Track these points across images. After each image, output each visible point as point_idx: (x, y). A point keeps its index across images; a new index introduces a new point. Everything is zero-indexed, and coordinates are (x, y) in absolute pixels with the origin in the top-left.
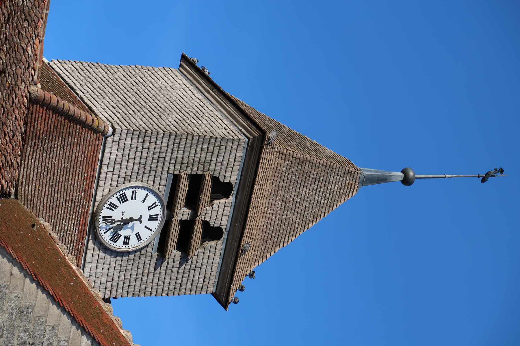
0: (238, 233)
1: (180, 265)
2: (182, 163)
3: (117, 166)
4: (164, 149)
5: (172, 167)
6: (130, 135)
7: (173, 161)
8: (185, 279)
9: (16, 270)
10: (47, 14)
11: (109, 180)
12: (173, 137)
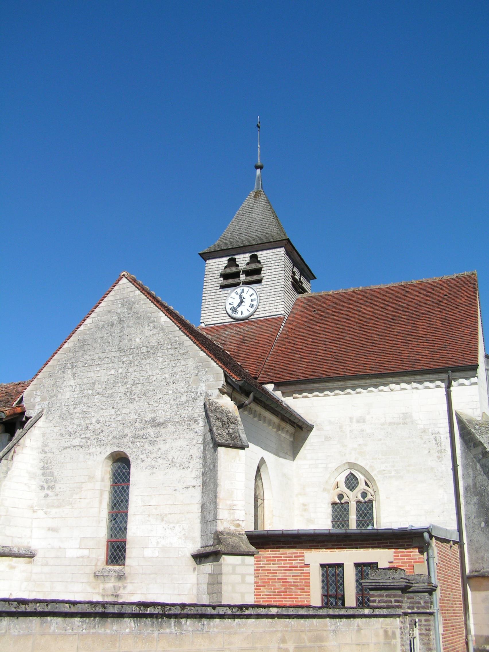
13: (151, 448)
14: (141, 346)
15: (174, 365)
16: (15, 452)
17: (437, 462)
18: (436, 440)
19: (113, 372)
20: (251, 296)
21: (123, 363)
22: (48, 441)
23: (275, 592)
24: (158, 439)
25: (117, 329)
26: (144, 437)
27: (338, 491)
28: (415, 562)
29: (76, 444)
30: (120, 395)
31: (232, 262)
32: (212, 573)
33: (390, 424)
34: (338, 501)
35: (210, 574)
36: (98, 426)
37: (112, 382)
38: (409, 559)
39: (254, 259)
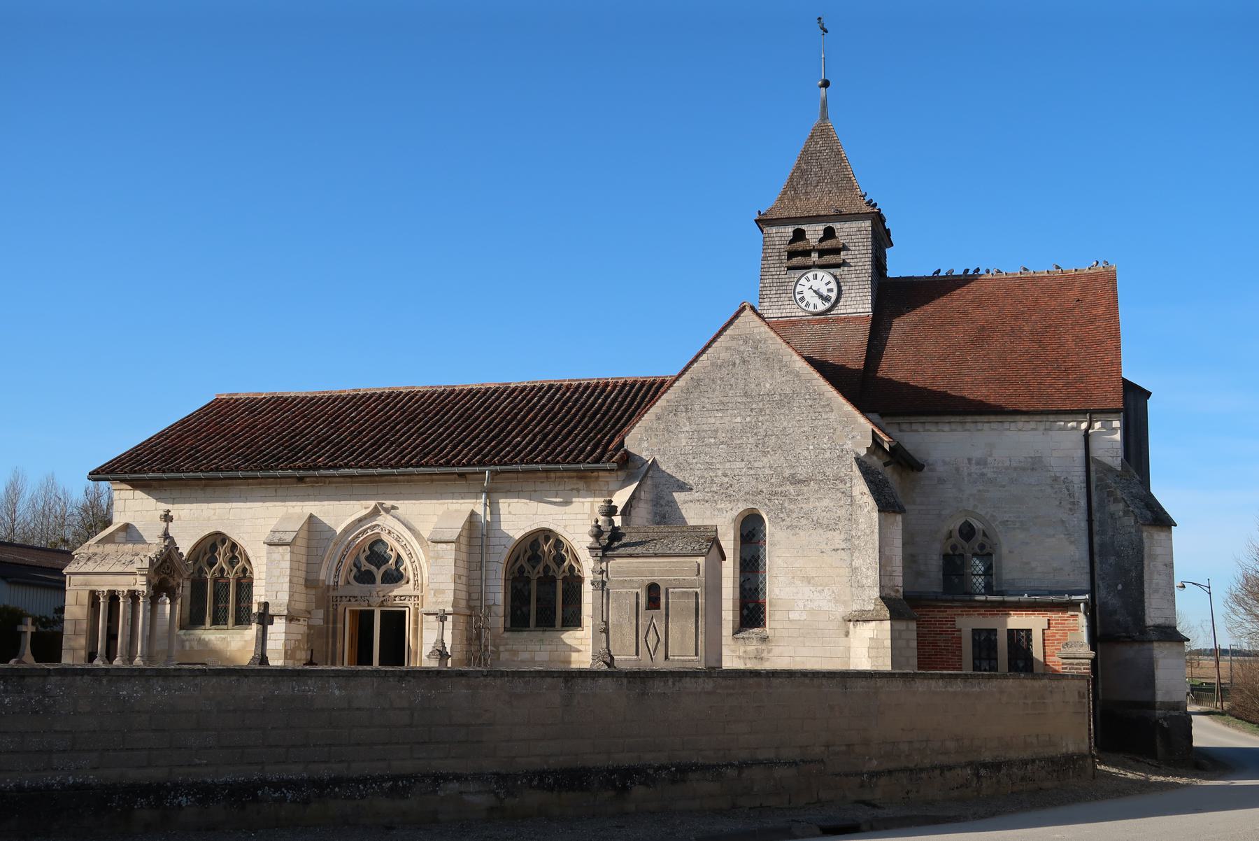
0: (825, 218)
1: (849, 250)
2: (779, 267)
3: (782, 307)
4: (771, 281)
5: (782, 273)
6: (762, 304)
7: (778, 273)
8: (860, 244)
9: (637, 425)
10: (670, 376)
11: (792, 310)
12: (763, 277)
13: (792, 507)
14: (773, 392)
15: (813, 418)
16: (631, 507)
17: (1069, 514)
18: (1068, 490)
19: (739, 419)
20: (827, 284)
21: (751, 410)
22: (663, 493)
23: (925, 655)
24: (799, 498)
25: (740, 370)
26: (783, 495)
27: (952, 540)
28: (1069, 630)
29: (700, 498)
30: (750, 446)
31: (799, 235)
32: (875, 637)
33: (1015, 469)
34: (951, 552)
35: (870, 638)
36: (726, 480)
37: (739, 431)
38: (1063, 627)
39: (829, 233)
